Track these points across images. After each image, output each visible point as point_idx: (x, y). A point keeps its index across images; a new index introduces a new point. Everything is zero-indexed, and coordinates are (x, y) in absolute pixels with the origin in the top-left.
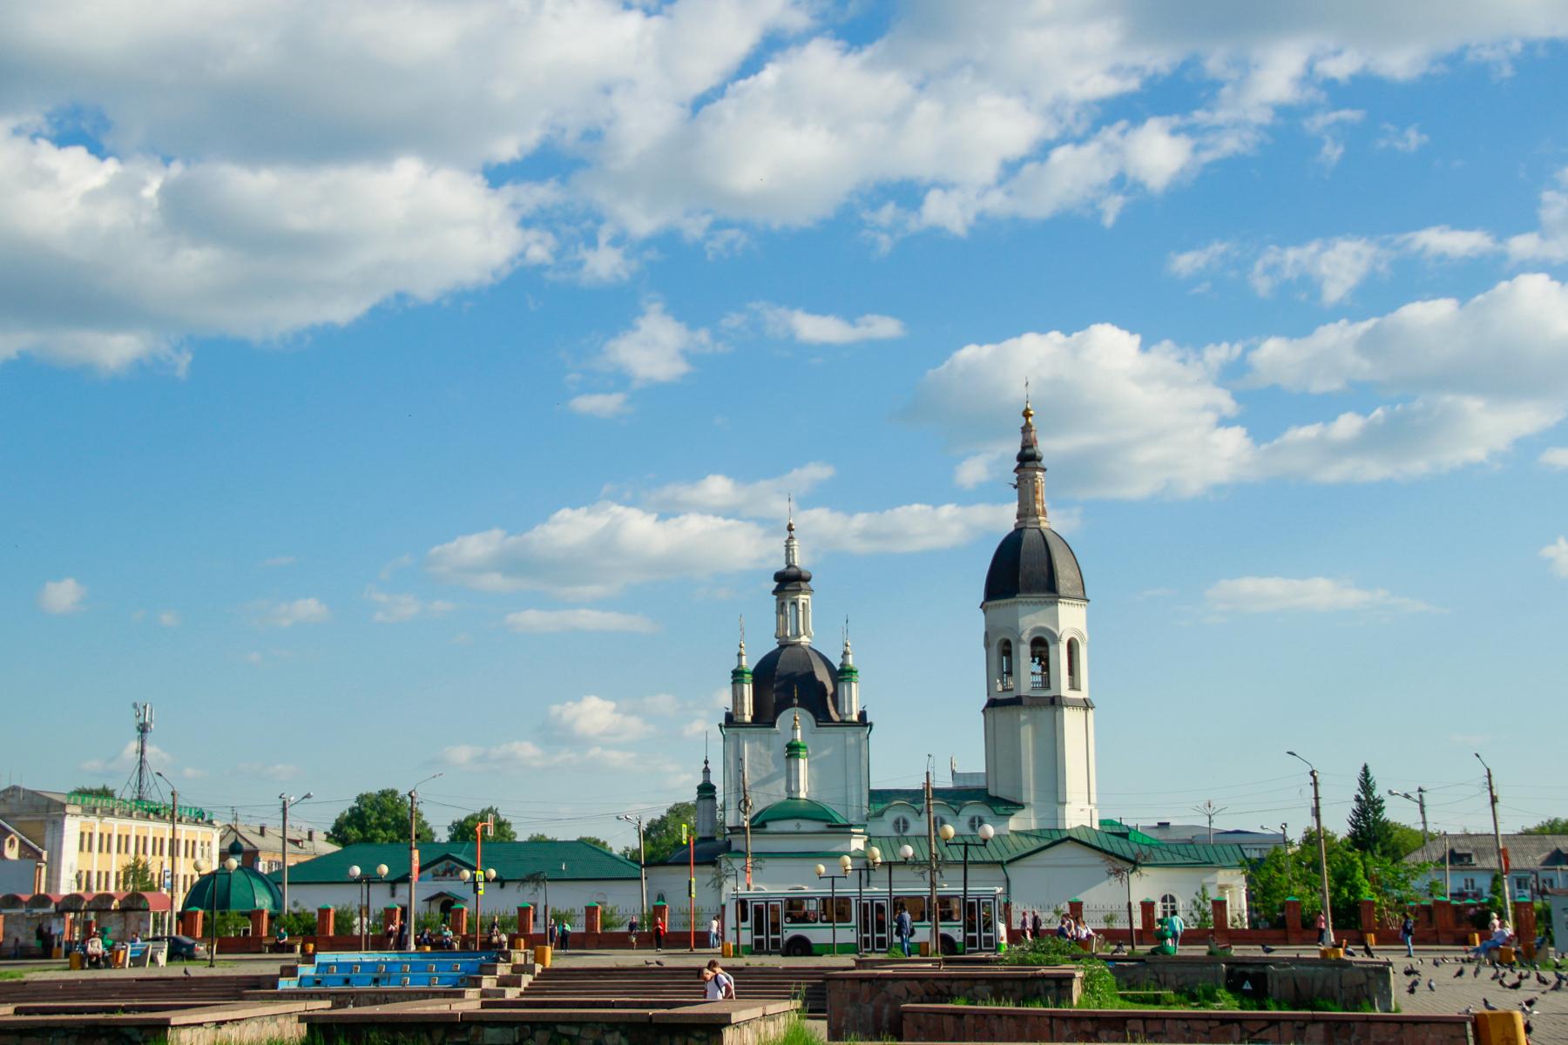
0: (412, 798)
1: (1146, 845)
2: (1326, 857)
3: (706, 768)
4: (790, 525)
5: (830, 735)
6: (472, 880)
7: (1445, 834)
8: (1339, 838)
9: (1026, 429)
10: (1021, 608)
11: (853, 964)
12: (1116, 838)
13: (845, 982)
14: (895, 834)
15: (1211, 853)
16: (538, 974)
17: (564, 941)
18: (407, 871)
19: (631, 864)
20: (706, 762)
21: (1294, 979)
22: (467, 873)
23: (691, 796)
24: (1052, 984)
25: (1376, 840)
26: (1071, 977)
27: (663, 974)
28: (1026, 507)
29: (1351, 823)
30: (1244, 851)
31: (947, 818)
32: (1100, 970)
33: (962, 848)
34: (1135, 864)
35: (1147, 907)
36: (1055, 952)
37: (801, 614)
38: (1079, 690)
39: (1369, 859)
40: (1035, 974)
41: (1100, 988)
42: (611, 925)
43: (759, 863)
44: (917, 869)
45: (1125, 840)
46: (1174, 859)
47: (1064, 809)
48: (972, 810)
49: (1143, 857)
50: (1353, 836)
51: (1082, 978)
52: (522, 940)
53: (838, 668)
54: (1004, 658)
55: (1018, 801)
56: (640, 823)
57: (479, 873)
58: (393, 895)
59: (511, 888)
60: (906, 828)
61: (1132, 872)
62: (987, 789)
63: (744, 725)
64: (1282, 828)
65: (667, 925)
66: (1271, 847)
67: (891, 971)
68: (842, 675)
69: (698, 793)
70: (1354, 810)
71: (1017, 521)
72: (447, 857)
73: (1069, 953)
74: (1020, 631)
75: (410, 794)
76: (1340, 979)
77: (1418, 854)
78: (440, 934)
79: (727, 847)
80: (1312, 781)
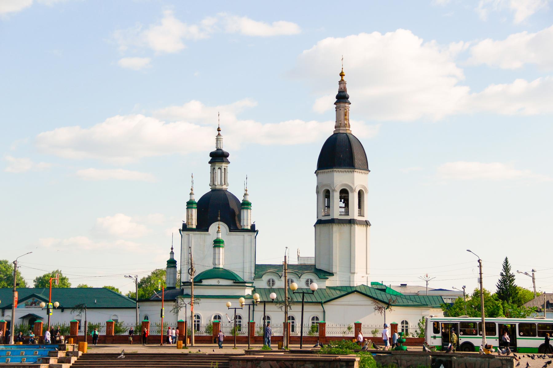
0: (15, 264)
1: (394, 295)
2: (484, 303)
3: (172, 251)
4: (219, 128)
5: (237, 237)
6: (46, 308)
7: (545, 293)
8: (491, 294)
9: (342, 82)
11: (243, 352)
12: (380, 291)
13: (239, 361)
14: (268, 287)
15: (427, 300)
16: (80, 357)
17: (94, 340)
18: (11, 303)
19: (131, 300)
20: (172, 249)
21: (465, 364)
22: (43, 304)
23: (164, 266)
24: (344, 364)
25: (510, 295)
26: (353, 361)
27: (146, 357)
28: (340, 122)
29: (498, 287)
30: (444, 299)
31: (294, 279)
32: (369, 357)
33: (301, 295)
34: (388, 305)
35: (394, 327)
36: (346, 348)
37: (223, 174)
38: (364, 216)
39: (506, 305)
40: (336, 359)
41: (368, 366)
43: (198, 301)
44: (278, 305)
45: (384, 293)
46: (413, 303)
47: (354, 276)
48: (306, 276)
49: (393, 301)
50: (498, 293)
51: (359, 361)
52: (72, 339)
53: (241, 202)
54: (326, 199)
55: (330, 272)
56: (137, 279)
57: (50, 304)
58: (3, 315)
59: (67, 313)
60: (273, 284)
61: (386, 309)
63: (192, 230)
64: (463, 288)
65: (151, 331)
66: (457, 297)
67: (262, 356)
68: (246, 205)
69: (167, 264)
70: (499, 280)
71: (335, 129)
72: (33, 296)
73: (353, 349)
74: (335, 186)
75: (14, 263)
76: (489, 363)
77: (531, 303)
78: (28, 335)
79: (181, 293)
80: (479, 265)
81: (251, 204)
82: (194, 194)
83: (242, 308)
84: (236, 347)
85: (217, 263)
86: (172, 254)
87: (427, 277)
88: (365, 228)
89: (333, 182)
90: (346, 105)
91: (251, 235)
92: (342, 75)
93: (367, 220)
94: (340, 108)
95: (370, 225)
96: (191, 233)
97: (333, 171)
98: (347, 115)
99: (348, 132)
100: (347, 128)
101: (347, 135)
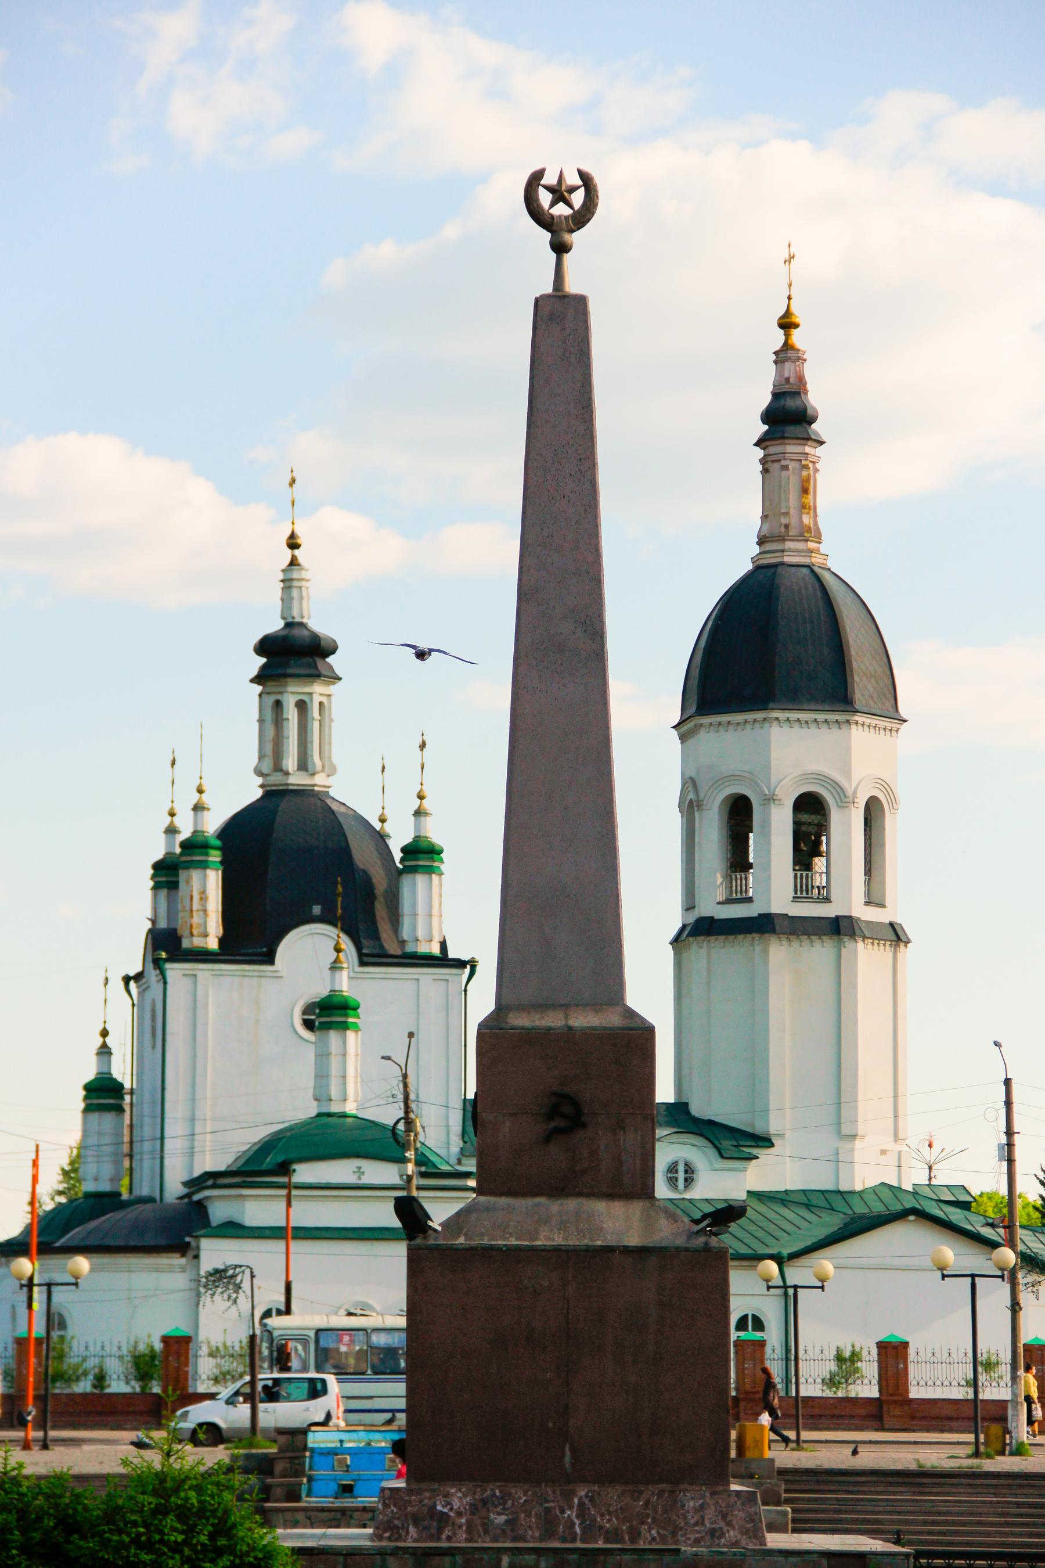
3: (104, 1045)
4: (293, 536)
9: (786, 354)
10: (775, 730)
20: (104, 1033)
28: (784, 521)
38: (883, 906)
42: (59, 1376)
55: (759, 1129)
60: (689, 1181)
62: (686, 1105)
63: (202, 956)
69: (86, 1098)
74: (773, 781)
81: (440, 852)
82: (208, 809)
83: (822, 1288)
84: (805, 1445)
85: (334, 1092)
86: (106, 1057)
87: (930, 1146)
88: (891, 955)
89: (767, 767)
90: (808, 450)
91: (447, 980)
92: (787, 324)
93: (892, 920)
94: (783, 463)
95: (907, 942)
96: (203, 970)
97: (765, 719)
98: (811, 490)
99: (816, 560)
100: (811, 545)
101: (813, 571)
